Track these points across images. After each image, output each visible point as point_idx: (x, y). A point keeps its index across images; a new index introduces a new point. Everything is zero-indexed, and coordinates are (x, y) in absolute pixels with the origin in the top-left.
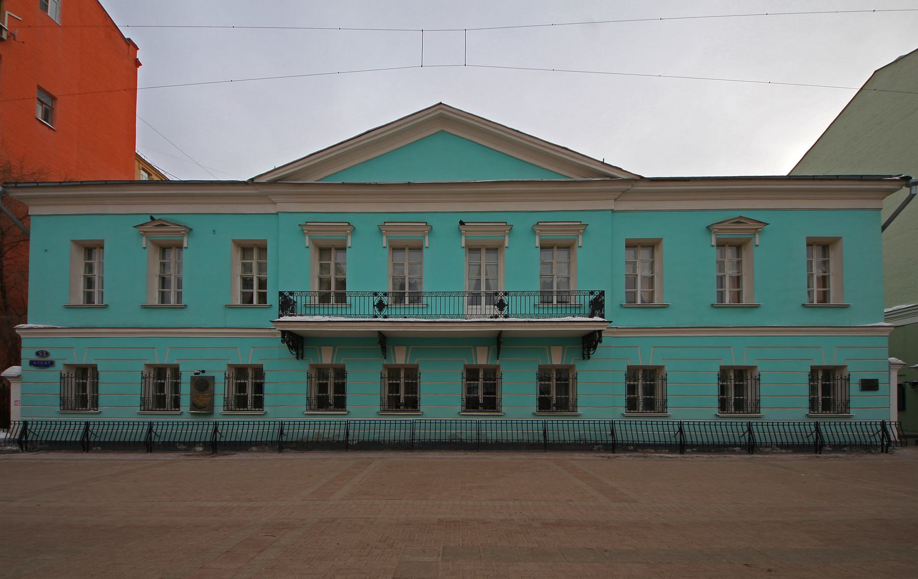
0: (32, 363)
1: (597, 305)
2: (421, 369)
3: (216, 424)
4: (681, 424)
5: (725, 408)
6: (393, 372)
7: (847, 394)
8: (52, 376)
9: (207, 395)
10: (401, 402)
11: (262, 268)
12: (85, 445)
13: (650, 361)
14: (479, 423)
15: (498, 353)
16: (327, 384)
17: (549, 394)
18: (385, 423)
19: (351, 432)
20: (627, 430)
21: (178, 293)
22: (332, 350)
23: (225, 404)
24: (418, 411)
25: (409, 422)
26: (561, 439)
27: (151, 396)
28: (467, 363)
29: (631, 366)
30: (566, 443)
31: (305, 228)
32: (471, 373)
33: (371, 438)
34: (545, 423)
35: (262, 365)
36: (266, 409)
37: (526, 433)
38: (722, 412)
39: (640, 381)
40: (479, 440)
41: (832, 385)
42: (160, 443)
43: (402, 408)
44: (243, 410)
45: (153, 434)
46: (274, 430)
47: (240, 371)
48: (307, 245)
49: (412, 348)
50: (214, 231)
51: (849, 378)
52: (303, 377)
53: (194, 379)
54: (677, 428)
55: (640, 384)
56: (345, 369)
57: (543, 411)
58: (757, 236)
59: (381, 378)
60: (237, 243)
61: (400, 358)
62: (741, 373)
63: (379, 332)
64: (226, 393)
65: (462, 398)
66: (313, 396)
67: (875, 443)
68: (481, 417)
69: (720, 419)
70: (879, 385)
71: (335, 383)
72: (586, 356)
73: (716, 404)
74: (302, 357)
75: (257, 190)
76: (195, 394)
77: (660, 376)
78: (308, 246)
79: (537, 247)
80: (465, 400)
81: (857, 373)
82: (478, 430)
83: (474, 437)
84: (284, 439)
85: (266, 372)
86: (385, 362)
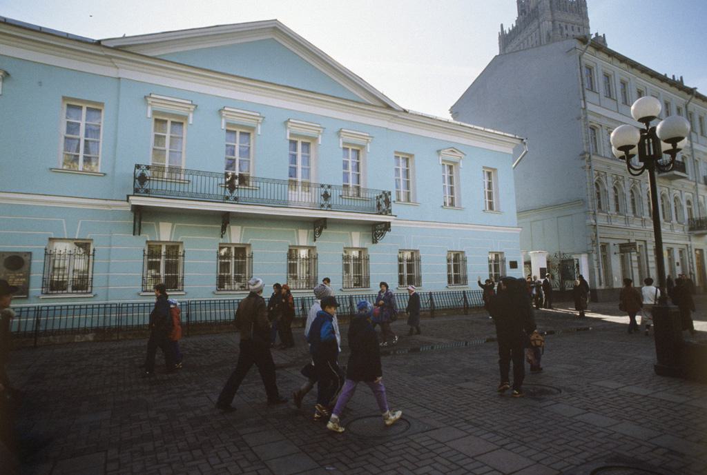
3: (38, 310)
5: (75, 290)
22: (170, 228)
25: (115, 306)
33: (135, 323)
39: (163, 257)
49: (246, 229)
61: (165, 232)
69: (216, 296)
72: (137, 232)
75: (102, 51)
81: (509, 258)
86: (221, 241)
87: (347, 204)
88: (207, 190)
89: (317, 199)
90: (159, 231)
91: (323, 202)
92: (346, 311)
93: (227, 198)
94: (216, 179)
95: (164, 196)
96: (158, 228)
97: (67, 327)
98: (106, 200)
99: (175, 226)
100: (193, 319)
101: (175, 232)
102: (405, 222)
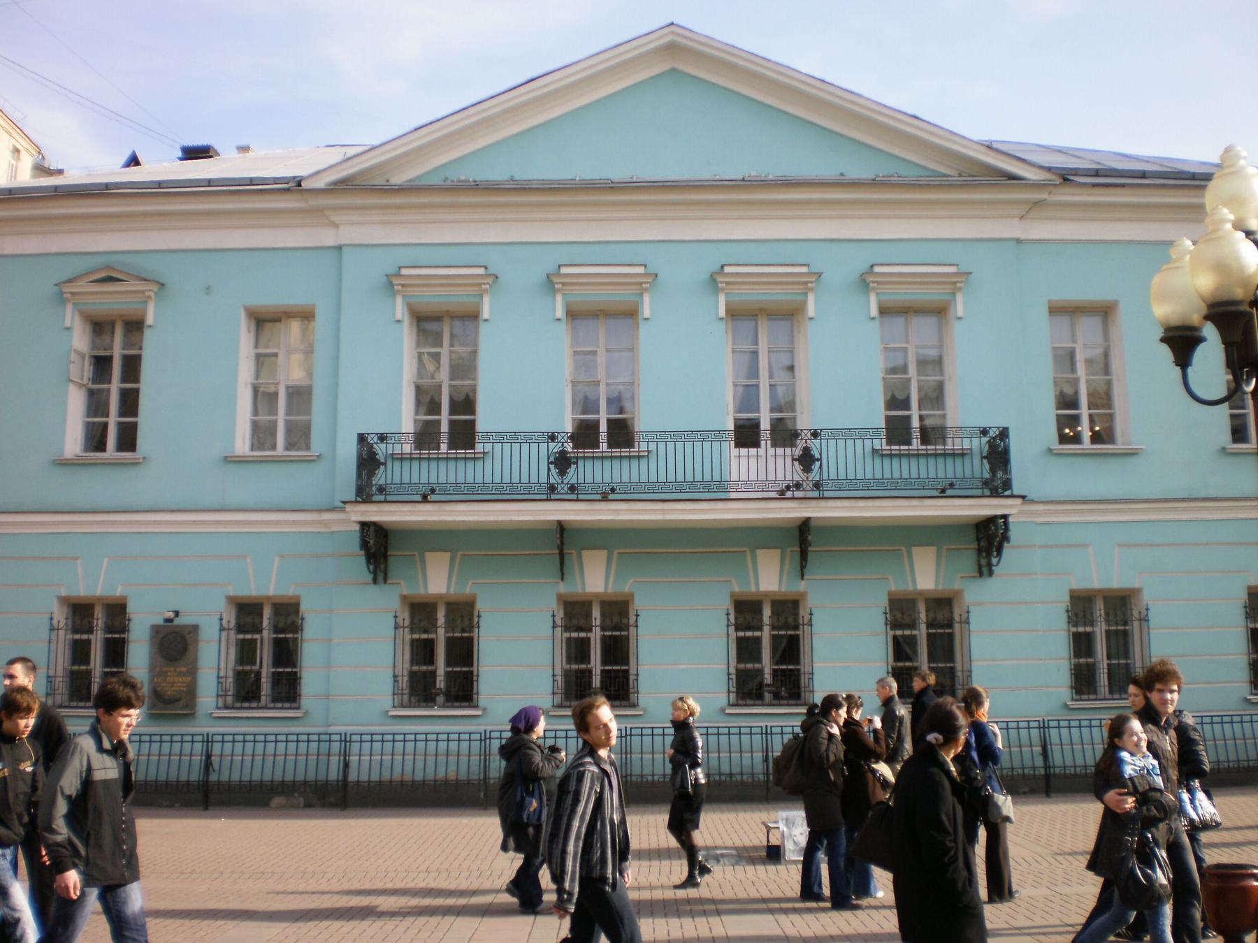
1: (998, 455)
2: (480, 605)
3: (208, 740)
4: (346, 740)
9: (184, 669)
10: (438, 686)
13: (1116, 581)
14: (767, 733)
15: (803, 567)
16: (589, 639)
17: (1127, 660)
19: (354, 759)
20: (1012, 744)
23: (220, 693)
24: (634, 706)
26: (656, 771)
27: (230, 674)
29: (1079, 590)
30: (645, 780)
36: (305, 702)
43: (440, 699)
46: (253, 755)
48: (399, 316)
52: (385, 627)
53: (157, 633)
55: (1100, 630)
63: (559, 522)
65: (554, 676)
66: (60, 672)
72: (985, 570)
76: (158, 669)
77: (1135, 613)
79: (559, 320)
80: (734, 677)
84: (213, 777)
85: (306, 616)
86: (563, 588)
87: (914, 475)
91: (555, 478)
93: (552, 488)
94: (859, 442)
96: (423, 562)
97: (286, 779)
99: (615, 555)
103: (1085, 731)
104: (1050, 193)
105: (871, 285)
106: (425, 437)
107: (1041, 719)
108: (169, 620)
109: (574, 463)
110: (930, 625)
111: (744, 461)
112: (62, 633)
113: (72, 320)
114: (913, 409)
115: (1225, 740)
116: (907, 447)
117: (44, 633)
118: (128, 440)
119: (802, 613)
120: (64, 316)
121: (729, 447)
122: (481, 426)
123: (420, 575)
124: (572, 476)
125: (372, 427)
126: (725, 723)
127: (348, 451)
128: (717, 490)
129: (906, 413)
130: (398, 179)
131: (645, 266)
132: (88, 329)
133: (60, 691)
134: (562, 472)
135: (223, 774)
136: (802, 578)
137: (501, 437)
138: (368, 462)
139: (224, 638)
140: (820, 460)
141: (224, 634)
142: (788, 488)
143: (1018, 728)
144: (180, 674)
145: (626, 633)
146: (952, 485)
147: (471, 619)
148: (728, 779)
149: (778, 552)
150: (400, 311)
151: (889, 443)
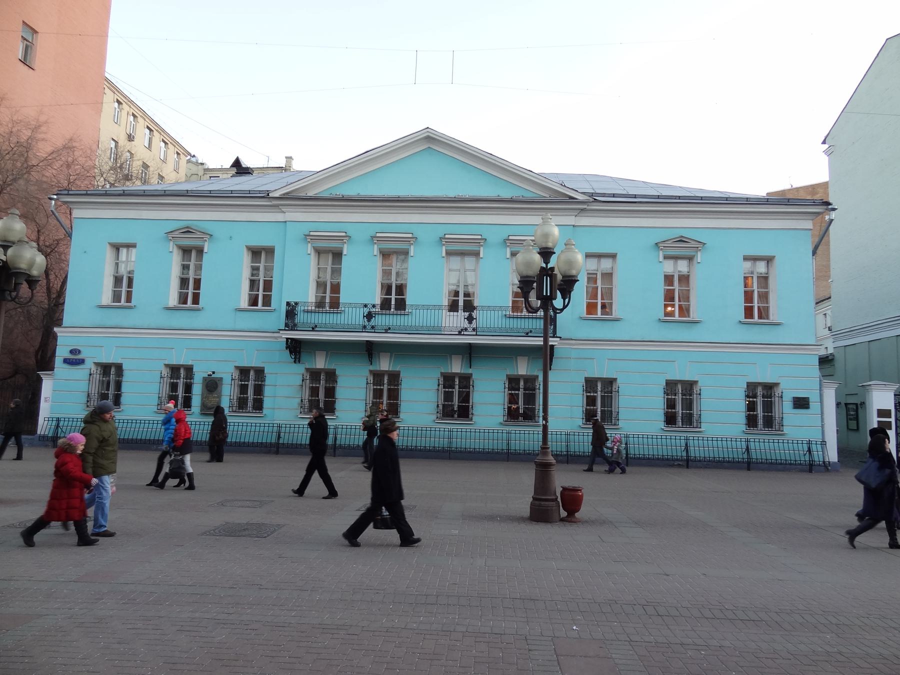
0: (66, 361)
4: (279, 426)
6: (378, 376)
7: (781, 412)
8: (80, 373)
11: (199, 268)
12: (688, 463)
14: (450, 431)
18: (238, 426)
19: (339, 436)
21: (128, 291)
25: (806, 442)
27: (235, 398)
28: (443, 371)
31: (308, 237)
32: (448, 380)
34: (748, 441)
35: (264, 368)
36: (265, 411)
37: (797, 453)
38: (749, 429)
40: (568, 451)
41: (773, 401)
42: (267, 444)
44: (242, 412)
45: (60, 430)
47: (244, 372)
48: (375, 253)
50: (231, 237)
51: (782, 395)
52: (298, 381)
53: (206, 380)
54: (806, 447)
56: (399, 374)
57: (527, 421)
58: (699, 254)
59: (664, 393)
60: (249, 248)
61: (385, 364)
62: (689, 387)
64: (232, 394)
65: (504, 408)
67: (780, 462)
68: (456, 426)
70: (810, 403)
71: (374, 388)
72: (297, 360)
73: (743, 420)
74: (299, 362)
78: (309, 253)
80: (506, 410)
81: (789, 390)
82: (450, 438)
83: (505, 447)
84: (281, 441)
86: (372, 368)
88: (485, 323)
89: (357, 320)
90: (451, 363)
92: (803, 459)
95: (396, 332)
98: (274, 332)
99: (393, 355)
100: (513, 448)
101: (394, 361)
102: (574, 342)
103: (762, 444)
104: (588, 205)
105: (661, 247)
106: (320, 304)
107: (808, 440)
108: (210, 375)
109: (374, 317)
110: (525, 389)
111: (451, 318)
112: (236, 381)
113: (173, 248)
114: (599, 299)
115: (727, 448)
116: (535, 314)
117: (158, 379)
118: (196, 300)
119: (614, 387)
120: (169, 247)
121: (445, 312)
122: (342, 300)
123: (314, 360)
124: (373, 322)
125: (292, 300)
126: (746, 436)
127: (284, 308)
128: (437, 330)
129: (390, 297)
130: (311, 193)
131: (346, 233)
132: (181, 253)
133: (235, 405)
134: (369, 321)
135: (285, 439)
136: (471, 368)
137: (417, 307)
138: (291, 312)
139: (233, 383)
140: (476, 319)
141: (233, 381)
142: (462, 330)
143: (588, 436)
144: (214, 397)
145: (383, 387)
146: (531, 331)
147: (398, 382)
148: (785, 462)
149: (461, 356)
150: (376, 252)
151: (513, 312)
